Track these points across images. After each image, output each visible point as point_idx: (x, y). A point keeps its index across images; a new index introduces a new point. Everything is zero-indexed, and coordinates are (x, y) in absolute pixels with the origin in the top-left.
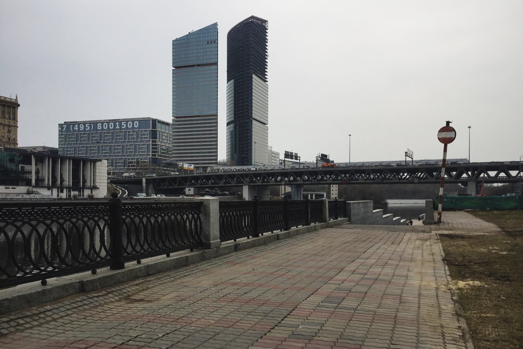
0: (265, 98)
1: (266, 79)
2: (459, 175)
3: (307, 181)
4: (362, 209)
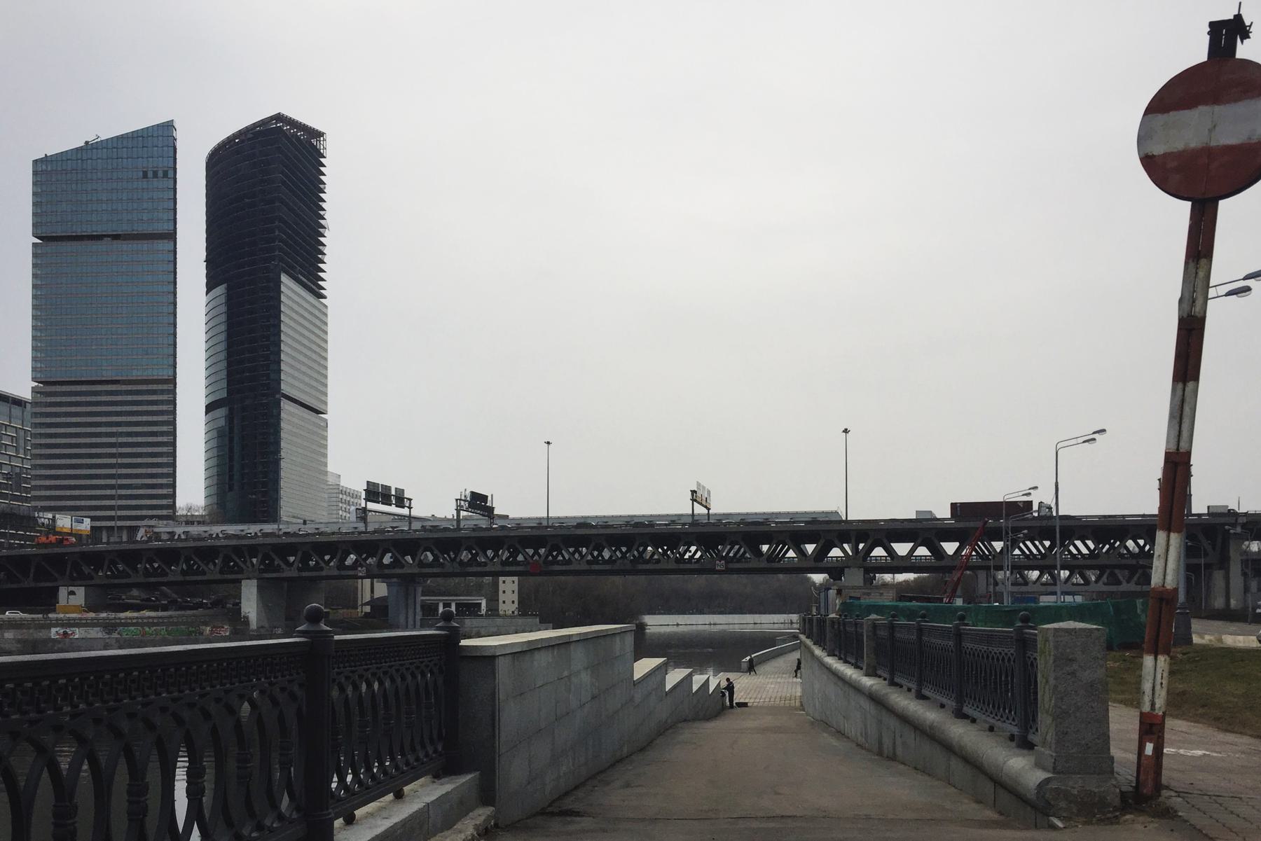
0: (318, 341)
1: (321, 291)
2: (822, 552)
3: (430, 565)
4: (585, 677)
